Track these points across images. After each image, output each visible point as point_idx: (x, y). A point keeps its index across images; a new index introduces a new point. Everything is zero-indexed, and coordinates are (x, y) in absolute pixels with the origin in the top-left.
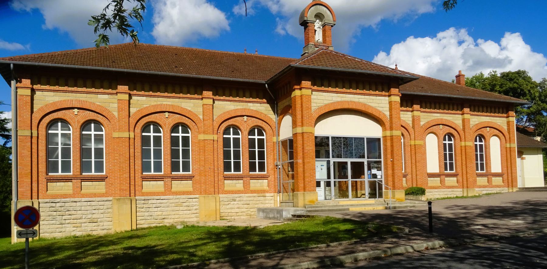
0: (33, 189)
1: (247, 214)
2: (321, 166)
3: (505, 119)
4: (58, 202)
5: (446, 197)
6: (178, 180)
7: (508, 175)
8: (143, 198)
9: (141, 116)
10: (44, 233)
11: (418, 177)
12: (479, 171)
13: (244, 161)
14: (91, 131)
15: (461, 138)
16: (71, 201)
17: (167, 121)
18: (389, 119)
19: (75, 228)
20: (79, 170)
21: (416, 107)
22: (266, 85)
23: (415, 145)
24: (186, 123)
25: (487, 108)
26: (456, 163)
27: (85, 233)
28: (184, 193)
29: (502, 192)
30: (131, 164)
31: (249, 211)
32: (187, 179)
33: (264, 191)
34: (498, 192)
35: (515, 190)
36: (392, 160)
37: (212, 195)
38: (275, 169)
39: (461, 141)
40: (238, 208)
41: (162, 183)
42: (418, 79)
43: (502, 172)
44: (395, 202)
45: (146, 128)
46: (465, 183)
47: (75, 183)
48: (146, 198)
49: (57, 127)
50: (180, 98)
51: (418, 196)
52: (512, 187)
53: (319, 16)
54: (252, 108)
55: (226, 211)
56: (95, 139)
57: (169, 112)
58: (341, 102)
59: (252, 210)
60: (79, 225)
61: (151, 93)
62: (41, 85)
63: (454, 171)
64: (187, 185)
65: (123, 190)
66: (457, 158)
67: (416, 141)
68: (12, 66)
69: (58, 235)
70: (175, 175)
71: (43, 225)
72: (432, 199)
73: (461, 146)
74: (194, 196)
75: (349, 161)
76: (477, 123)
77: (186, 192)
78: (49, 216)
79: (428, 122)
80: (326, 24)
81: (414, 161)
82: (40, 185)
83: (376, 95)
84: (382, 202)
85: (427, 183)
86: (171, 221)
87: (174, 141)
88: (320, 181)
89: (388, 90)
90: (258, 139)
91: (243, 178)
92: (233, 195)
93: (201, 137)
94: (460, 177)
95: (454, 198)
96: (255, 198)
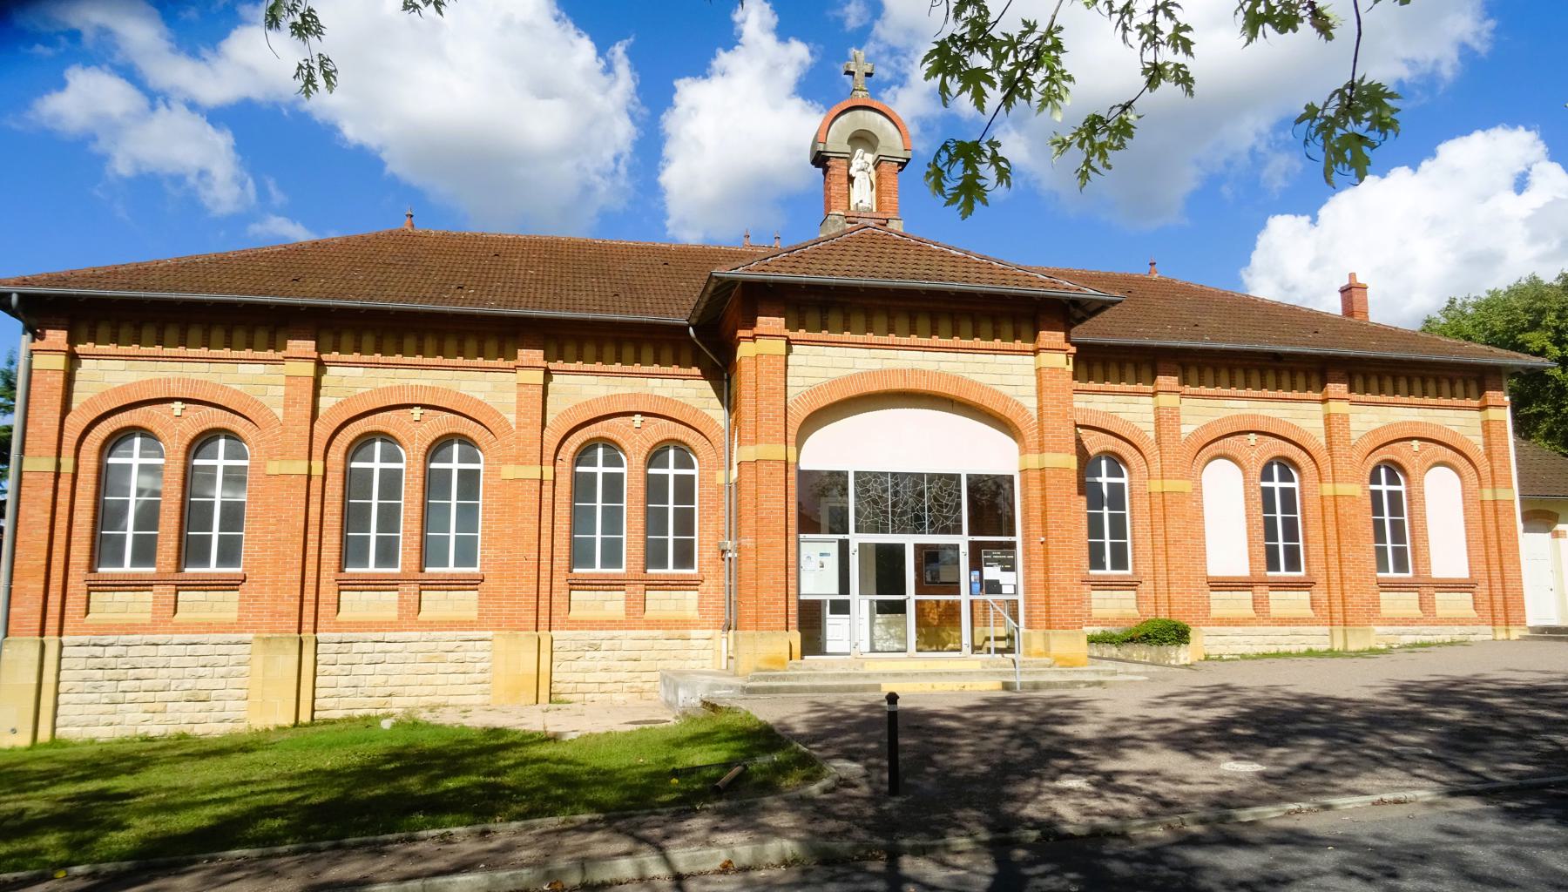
0: (49, 608)
1: (632, 687)
2: (822, 555)
3: (1476, 414)
4: (111, 645)
5: (1273, 650)
6: (439, 590)
7: (1490, 586)
8: (337, 636)
9: (345, 418)
10: (66, 726)
11: (1174, 589)
12: (1391, 574)
13: (632, 538)
14: (667, 466)
15: (1480, 479)
16: (144, 642)
17: (417, 431)
18: (1036, 420)
19: (148, 716)
20: (641, 562)
21: (1337, 389)
22: (691, 329)
23: (1495, 501)
24: (470, 434)
25: (1308, 377)
26: (1306, 548)
27: (172, 730)
28: (452, 625)
29: (1472, 638)
30: (310, 544)
31: (638, 680)
32: (464, 587)
33: (685, 624)
34: (1458, 638)
35: (1515, 633)
36: (1043, 539)
37: (527, 633)
38: (720, 561)
39: (1321, 481)
40: (606, 670)
41: (393, 596)
42: (1120, 302)
43: (1471, 577)
44: (1050, 666)
45: (585, 453)
46: (1338, 608)
47: (160, 593)
48: (346, 636)
49: (132, 447)
50: (455, 368)
51: (1164, 648)
52: (1507, 624)
53: (862, 139)
54: (658, 392)
55: (569, 677)
56: (225, 479)
57: (423, 406)
58: (883, 373)
59: (645, 676)
60: (159, 706)
61: (378, 357)
62: (96, 344)
63: (1410, 574)
64: (464, 603)
65: (281, 615)
66: (1311, 533)
67: (1165, 481)
68: (14, 298)
69: (103, 734)
70: (194, 574)
71: (67, 703)
72: (1225, 657)
73: (1322, 498)
74: (478, 633)
75: (909, 541)
76: (1378, 425)
77: (458, 622)
78: (84, 680)
79: (1207, 426)
80: (881, 158)
81: (1160, 541)
82: (70, 599)
83: (995, 351)
84: (1005, 666)
85: (1208, 607)
86: (411, 702)
87: (655, 488)
88: (800, 602)
89: (1034, 338)
90: (677, 477)
91: (152, 585)
92: (592, 632)
93: (509, 471)
94: (1320, 592)
95: (1299, 655)
96: (658, 644)
